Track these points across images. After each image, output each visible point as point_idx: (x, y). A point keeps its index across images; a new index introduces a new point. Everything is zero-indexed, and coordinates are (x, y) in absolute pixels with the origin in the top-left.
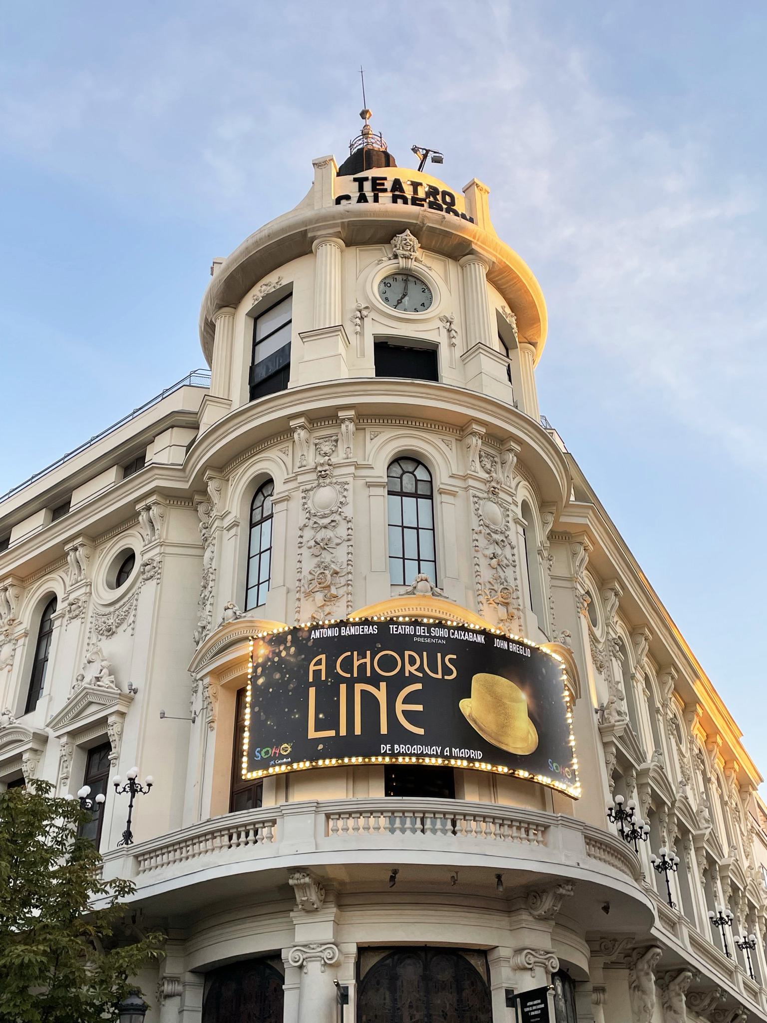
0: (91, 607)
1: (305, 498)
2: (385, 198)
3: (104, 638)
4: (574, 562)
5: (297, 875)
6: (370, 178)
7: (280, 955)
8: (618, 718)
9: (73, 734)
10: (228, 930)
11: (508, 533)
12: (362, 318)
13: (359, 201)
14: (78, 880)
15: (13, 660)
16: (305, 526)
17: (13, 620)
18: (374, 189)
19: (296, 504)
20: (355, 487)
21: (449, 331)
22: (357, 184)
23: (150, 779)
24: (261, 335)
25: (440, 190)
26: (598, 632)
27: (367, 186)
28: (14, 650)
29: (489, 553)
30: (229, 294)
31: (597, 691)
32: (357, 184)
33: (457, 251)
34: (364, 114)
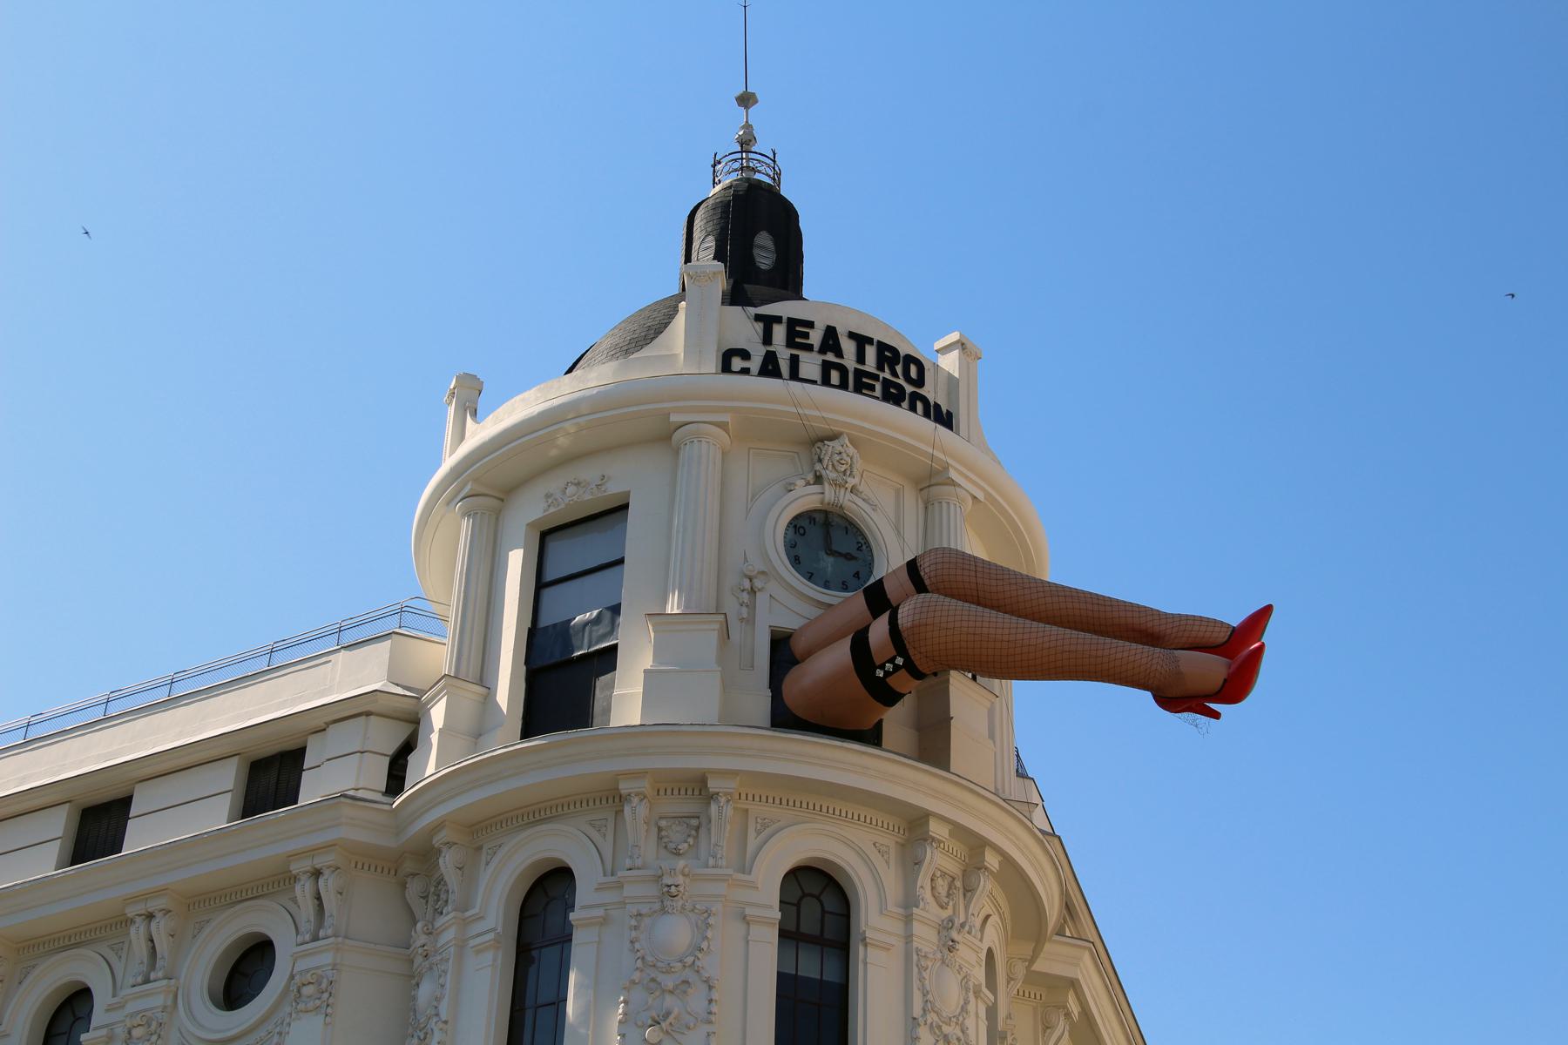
1: (636, 928)
12: (753, 591)
18: (790, 343)
25: (902, 354)
27: (779, 332)
32: (760, 326)
34: (746, 100)
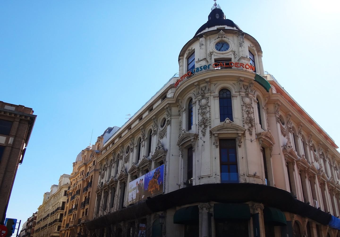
0: (158, 132)
8: (289, 148)
11: (251, 105)
14: (164, 193)
20: (212, 99)
21: (234, 54)
24: (189, 62)
28: (145, 142)
31: (282, 140)
33: (244, 103)
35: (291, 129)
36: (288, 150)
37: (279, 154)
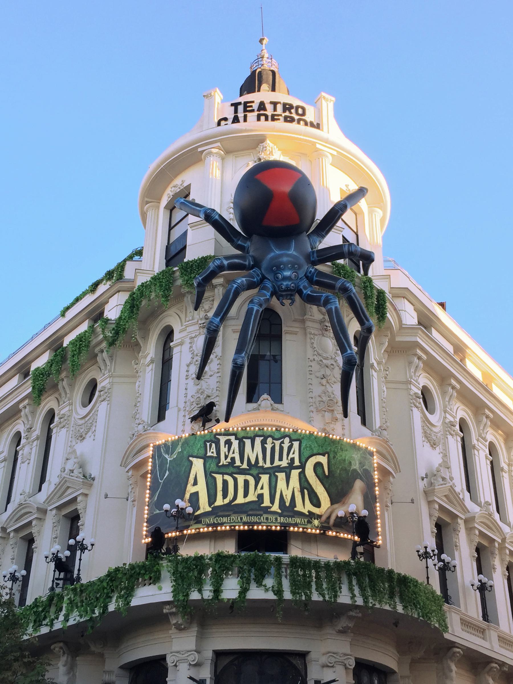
2: (252, 116)
3: (79, 441)
4: (410, 369)
5: (168, 607)
6: (243, 102)
7: (166, 658)
8: (442, 482)
9: (59, 508)
10: (156, 637)
13: (233, 122)
15: (30, 456)
16: (190, 363)
17: (31, 428)
18: (245, 111)
19: (186, 347)
22: (233, 107)
23: (92, 541)
25: (294, 105)
26: (433, 418)
28: (31, 449)
29: (320, 374)
30: (151, 193)
35: (454, 426)
36: (440, 488)
37: (412, 501)
